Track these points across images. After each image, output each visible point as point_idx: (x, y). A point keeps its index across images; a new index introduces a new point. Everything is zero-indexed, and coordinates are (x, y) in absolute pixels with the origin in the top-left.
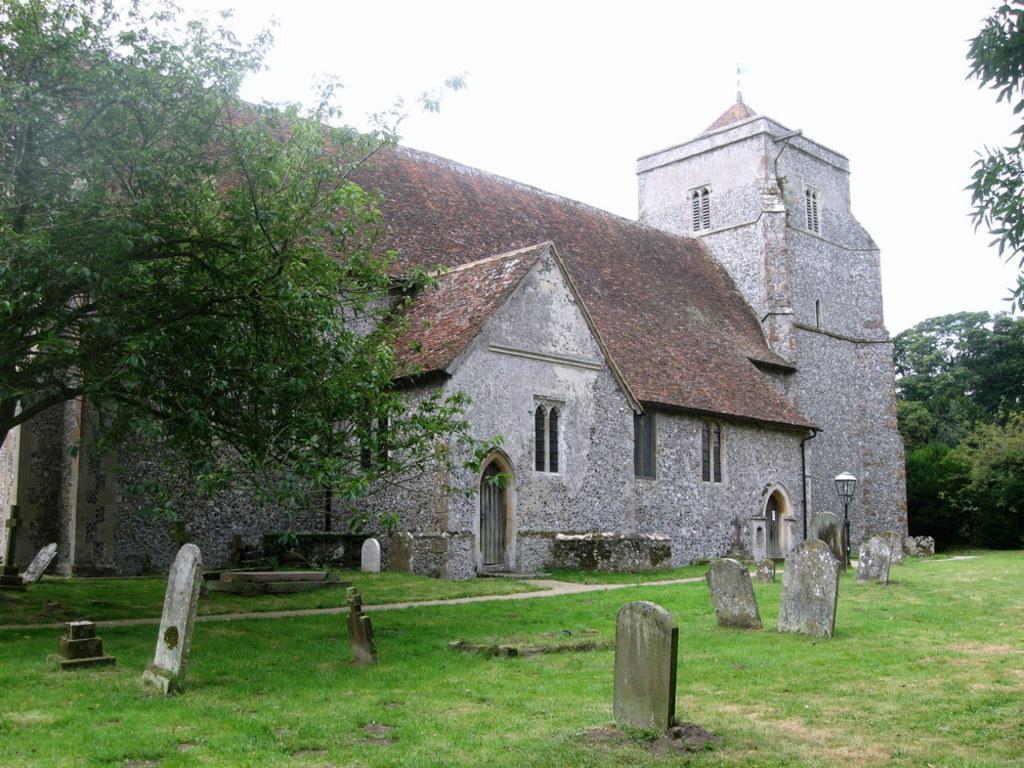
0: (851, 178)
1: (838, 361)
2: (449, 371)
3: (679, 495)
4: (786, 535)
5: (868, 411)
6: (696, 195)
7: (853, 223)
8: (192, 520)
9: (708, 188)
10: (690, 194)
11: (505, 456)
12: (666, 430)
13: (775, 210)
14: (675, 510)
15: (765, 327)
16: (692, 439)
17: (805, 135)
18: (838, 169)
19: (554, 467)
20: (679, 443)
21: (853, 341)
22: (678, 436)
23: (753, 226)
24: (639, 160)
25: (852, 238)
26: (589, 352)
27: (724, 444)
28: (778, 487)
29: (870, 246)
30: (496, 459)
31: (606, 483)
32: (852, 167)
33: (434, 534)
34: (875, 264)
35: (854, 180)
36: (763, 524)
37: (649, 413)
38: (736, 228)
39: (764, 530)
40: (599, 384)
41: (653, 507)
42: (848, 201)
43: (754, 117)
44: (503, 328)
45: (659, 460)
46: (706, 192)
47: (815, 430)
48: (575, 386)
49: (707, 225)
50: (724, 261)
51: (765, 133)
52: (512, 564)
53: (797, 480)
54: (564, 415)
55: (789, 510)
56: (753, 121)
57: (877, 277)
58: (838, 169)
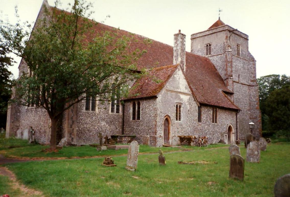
0: (249, 41)
1: (244, 91)
2: (157, 96)
3: (207, 126)
4: (232, 137)
5: (252, 104)
6: (207, 46)
7: (249, 53)
8: (92, 132)
9: (211, 44)
10: (206, 45)
11: (169, 117)
12: (204, 110)
13: (229, 51)
14: (205, 130)
15: (225, 82)
16: (210, 112)
17: (238, 30)
18: (245, 39)
19: (180, 120)
20: (207, 114)
21: (248, 85)
22: (207, 111)
23: (223, 55)
24: (191, 35)
25: (249, 57)
26: (188, 91)
27: (218, 113)
28: (230, 125)
29: (253, 60)
30: (230, 126)
31: (191, 124)
32: (249, 38)
33: (153, 136)
34: (255, 65)
35: (249, 42)
36: (227, 135)
37: (202, 105)
38: (218, 55)
39: (227, 136)
40: (190, 99)
41: (200, 130)
42: (248, 48)
43: (224, 25)
44: (168, 86)
45: (202, 117)
46: (210, 45)
47: (240, 110)
48: (185, 99)
49: (210, 54)
50: (215, 63)
51: (227, 30)
52: (170, 144)
53: (235, 123)
54: (182, 106)
55: (234, 130)
56: (223, 26)
57: (255, 68)
58: (245, 39)
